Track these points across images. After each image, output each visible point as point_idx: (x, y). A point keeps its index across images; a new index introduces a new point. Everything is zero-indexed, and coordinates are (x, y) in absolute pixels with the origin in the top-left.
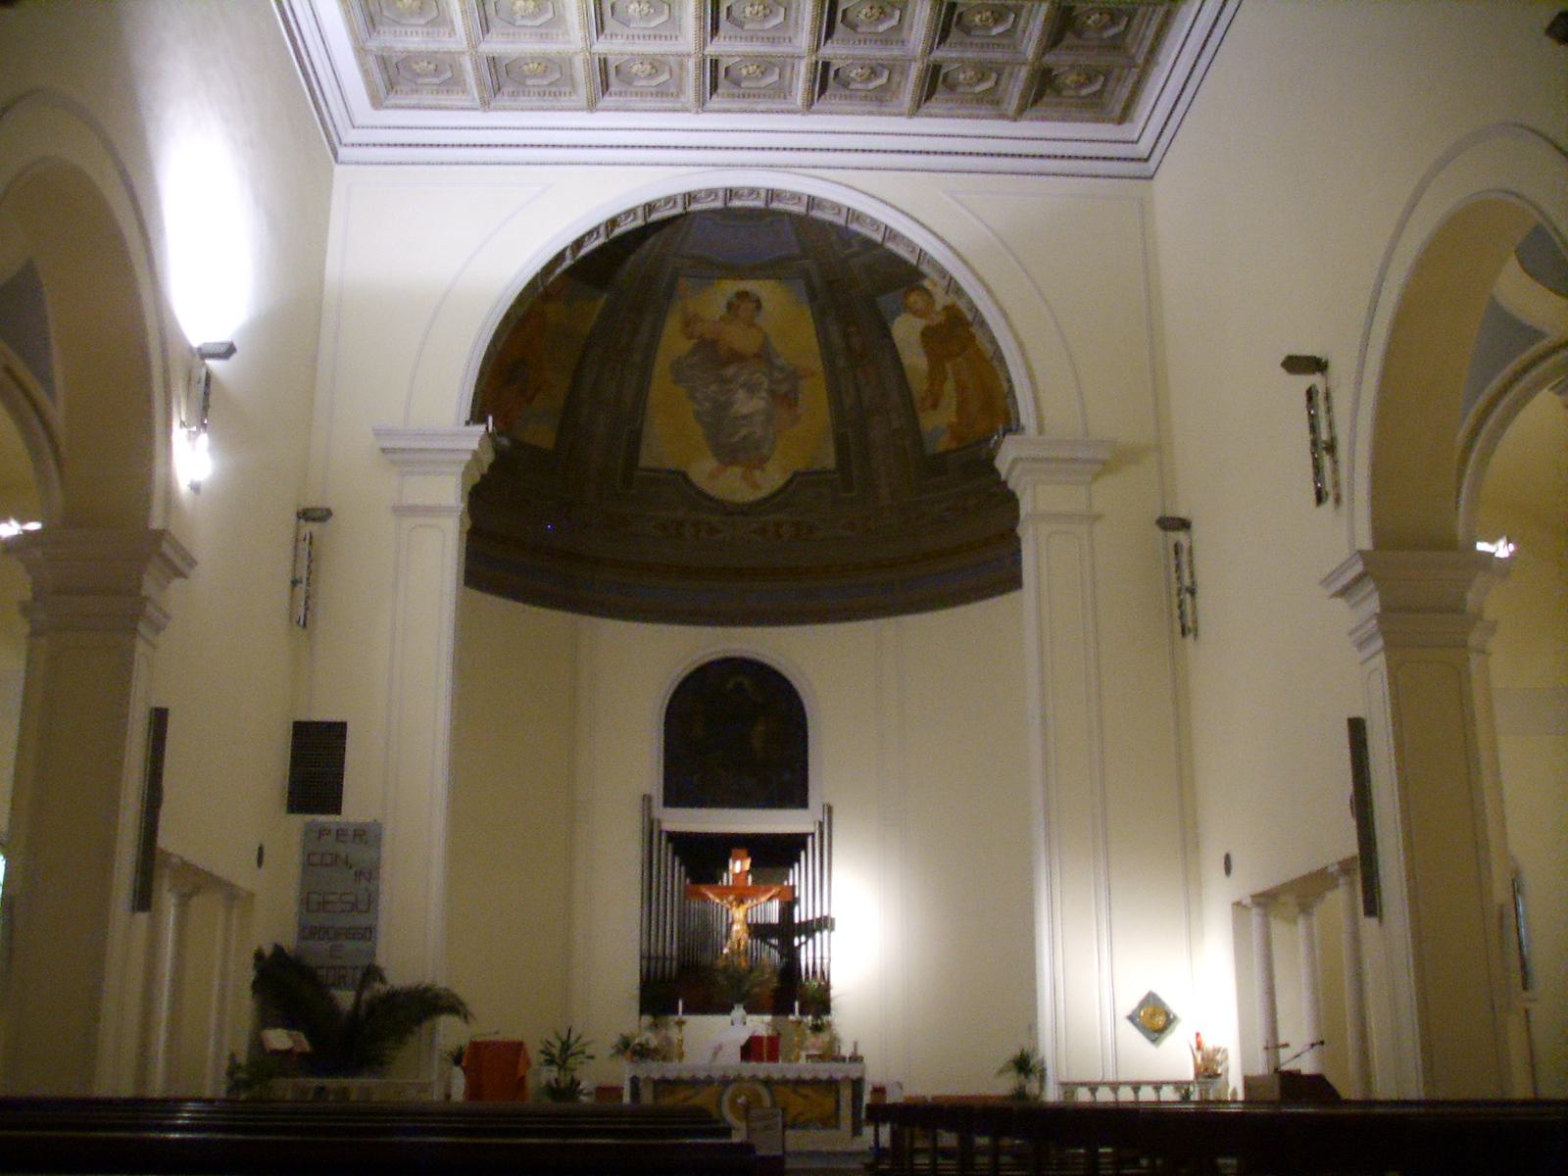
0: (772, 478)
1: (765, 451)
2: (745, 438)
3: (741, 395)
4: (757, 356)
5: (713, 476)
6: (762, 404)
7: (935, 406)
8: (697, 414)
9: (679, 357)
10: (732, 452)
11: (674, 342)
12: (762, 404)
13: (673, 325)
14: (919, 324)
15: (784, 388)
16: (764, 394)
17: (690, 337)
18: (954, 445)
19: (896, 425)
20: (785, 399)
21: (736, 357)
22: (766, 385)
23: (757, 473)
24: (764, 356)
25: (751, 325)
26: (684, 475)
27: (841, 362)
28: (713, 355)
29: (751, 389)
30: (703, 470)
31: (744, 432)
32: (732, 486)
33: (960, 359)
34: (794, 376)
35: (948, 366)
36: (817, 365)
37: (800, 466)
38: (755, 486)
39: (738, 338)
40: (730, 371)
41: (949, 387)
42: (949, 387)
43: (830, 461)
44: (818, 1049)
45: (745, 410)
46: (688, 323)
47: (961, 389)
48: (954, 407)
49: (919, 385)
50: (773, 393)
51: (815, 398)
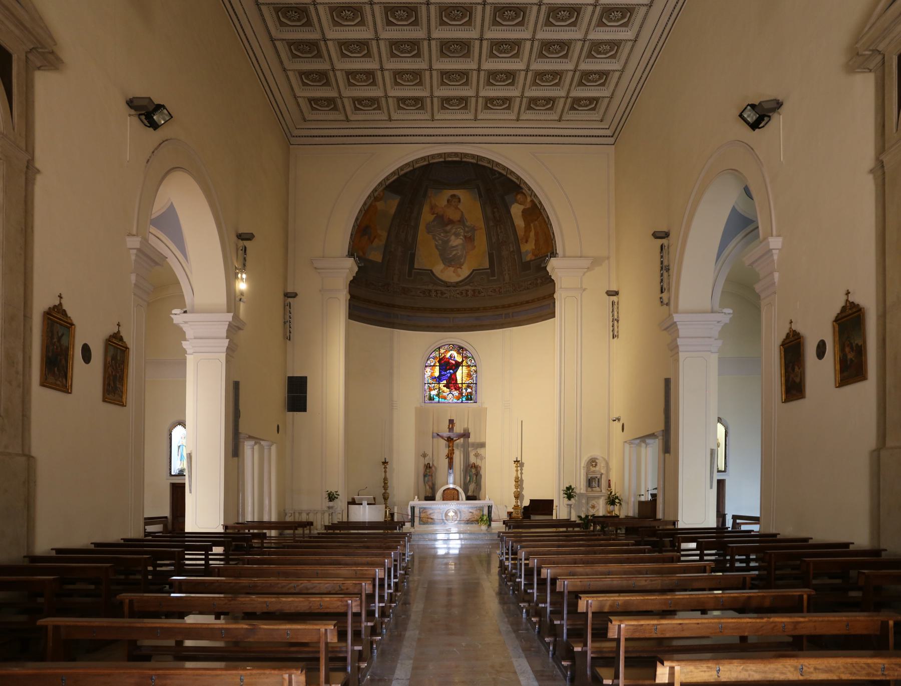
0: (465, 272)
3: (453, 237)
4: (459, 221)
5: (442, 271)
7: (527, 242)
8: (436, 246)
11: (427, 216)
13: (426, 209)
14: (522, 207)
15: (469, 234)
20: (469, 239)
21: (451, 222)
24: (462, 221)
25: (457, 208)
26: (431, 271)
27: (491, 224)
28: (443, 222)
29: (457, 235)
31: (454, 253)
32: (451, 275)
34: (473, 229)
40: (449, 228)
41: (532, 234)
42: (532, 234)
45: (455, 244)
46: (433, 208)
47: (536, 234)
49: (521, 233)
50: (465, 237)
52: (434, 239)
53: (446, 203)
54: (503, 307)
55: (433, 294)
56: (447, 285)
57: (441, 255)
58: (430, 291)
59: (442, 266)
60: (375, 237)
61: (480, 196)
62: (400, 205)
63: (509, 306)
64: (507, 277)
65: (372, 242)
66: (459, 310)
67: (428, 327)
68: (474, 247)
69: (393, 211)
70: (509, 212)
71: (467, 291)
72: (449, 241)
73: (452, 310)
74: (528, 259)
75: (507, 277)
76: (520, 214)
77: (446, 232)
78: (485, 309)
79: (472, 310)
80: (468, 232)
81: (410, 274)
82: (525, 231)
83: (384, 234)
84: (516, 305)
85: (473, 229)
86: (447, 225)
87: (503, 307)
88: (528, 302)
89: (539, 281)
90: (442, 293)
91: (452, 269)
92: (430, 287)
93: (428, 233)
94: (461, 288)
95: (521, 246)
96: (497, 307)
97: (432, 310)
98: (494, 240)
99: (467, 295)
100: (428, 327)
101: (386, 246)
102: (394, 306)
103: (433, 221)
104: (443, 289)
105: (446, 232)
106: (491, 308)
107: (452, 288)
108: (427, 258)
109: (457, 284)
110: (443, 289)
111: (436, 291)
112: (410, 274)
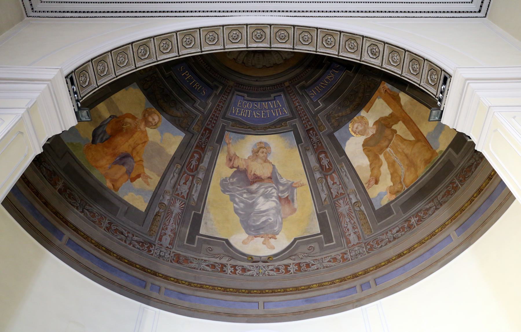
0: (281, 243)
1: (276, 228)
2: (264, 222)
3: (261, 200)
4: (270, 178)
5: (244, 242)
6: (273, 204)
7: (377, 182)
8: (236, 211)
9: (226, 178)
10: (254, 230)
11: (222, 170)
12: (273, 204)
13: (222, 159)
14: (361, 139)
15: (286, 194)
16: (274, 199)
17: (232, 167)
18: (393, 197)
19: (354, 201)
20: (287, 200)
21: (258, 179)
22: (275, 195)
23: (272, 240)
24: (273, 178)
25: (266, 161)
26: (227, 241)
27: (317, 175)
28: (245, 178)
29: (267, 196)
30: (239, 240)
31: (264, 219)
32: (258, 247)
33: (388, 149)
34: (292, 187)
35: (382, 157)
36: (305, 181)
37: (299, 235)
38: (273, 248)
39: (259, 169)
40: (254, 187)
41: (385, 168)
42: (385, 168)
43: (316, 229)
44: (397, 99)
45: (263, 208)
46: (230, 159)
47: (392, 165)
48: (389, 177)
49: (364, 175)
50: (279, 198)
51: (304, 199)
52: (233, 200)
53: (250, 154)
54: (355, 276)
55: (229, 270)
56: (252, 259)
57: (242, 222)
58: (223, 266)
59: (244, 236)
60: (138, 176)
61: (299, 141)
62: (184, 146)
63: (366, 272)
64: (353, 238)
65: (133, 180)
66: (273, 292)
67: (218, 313)
68: (295, 210)
69: (172, 150)
70: (342, 153)
71: (287, 266)
72: (253, 205)
73: (262, 292)
74: (385, 201)
75: (353, 238)
76: (361, 148)
77: (251, 192)
78: (321, 285)
79: (297, 289)
80: (283, 192)
81: (191, 240)
82: (372, 170)
83: (155, 179)
84: (378, 267)
85: (292, 187)
86: (252, 183)
87: (355, 276)
88: (400, 256)
89: (413, 220)
90: (244, 270)
91: (260, 240)
92: (224, 261)
93: (224, 191)
94: (277, 264)
95: (368, 191)
96: (343, 280)
97: (225, 290)
98: (323, 196)
99: (287, 271)
100: (218, 313)
101: (155, 195)
102: (155, 274)
103: (233, 176)
104: (246, 264)
105: (251, 192)
106: (333, 282)
107: (261, 264)
108: (220, 219)
109: (269, 259)
110: (246, 264)
111: (234, 267)
112: (191, 240)
